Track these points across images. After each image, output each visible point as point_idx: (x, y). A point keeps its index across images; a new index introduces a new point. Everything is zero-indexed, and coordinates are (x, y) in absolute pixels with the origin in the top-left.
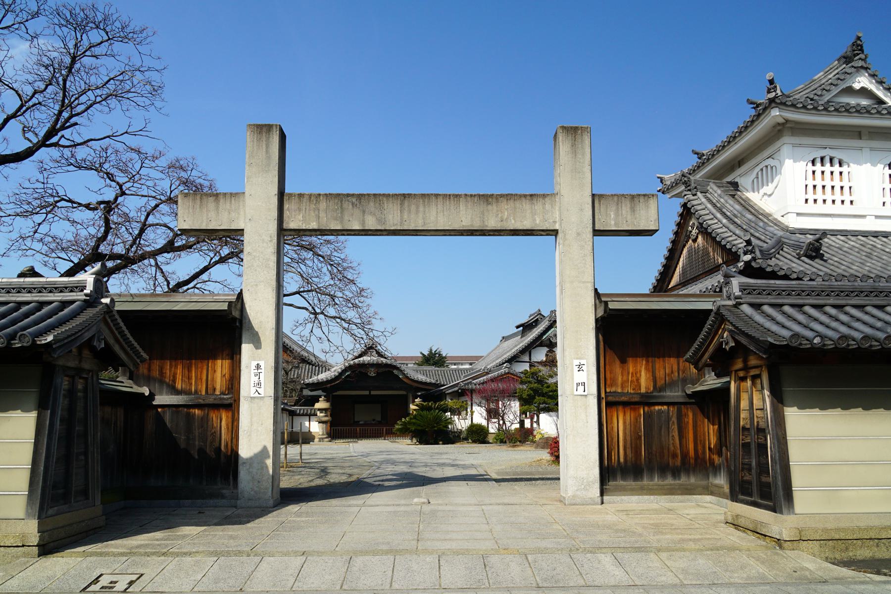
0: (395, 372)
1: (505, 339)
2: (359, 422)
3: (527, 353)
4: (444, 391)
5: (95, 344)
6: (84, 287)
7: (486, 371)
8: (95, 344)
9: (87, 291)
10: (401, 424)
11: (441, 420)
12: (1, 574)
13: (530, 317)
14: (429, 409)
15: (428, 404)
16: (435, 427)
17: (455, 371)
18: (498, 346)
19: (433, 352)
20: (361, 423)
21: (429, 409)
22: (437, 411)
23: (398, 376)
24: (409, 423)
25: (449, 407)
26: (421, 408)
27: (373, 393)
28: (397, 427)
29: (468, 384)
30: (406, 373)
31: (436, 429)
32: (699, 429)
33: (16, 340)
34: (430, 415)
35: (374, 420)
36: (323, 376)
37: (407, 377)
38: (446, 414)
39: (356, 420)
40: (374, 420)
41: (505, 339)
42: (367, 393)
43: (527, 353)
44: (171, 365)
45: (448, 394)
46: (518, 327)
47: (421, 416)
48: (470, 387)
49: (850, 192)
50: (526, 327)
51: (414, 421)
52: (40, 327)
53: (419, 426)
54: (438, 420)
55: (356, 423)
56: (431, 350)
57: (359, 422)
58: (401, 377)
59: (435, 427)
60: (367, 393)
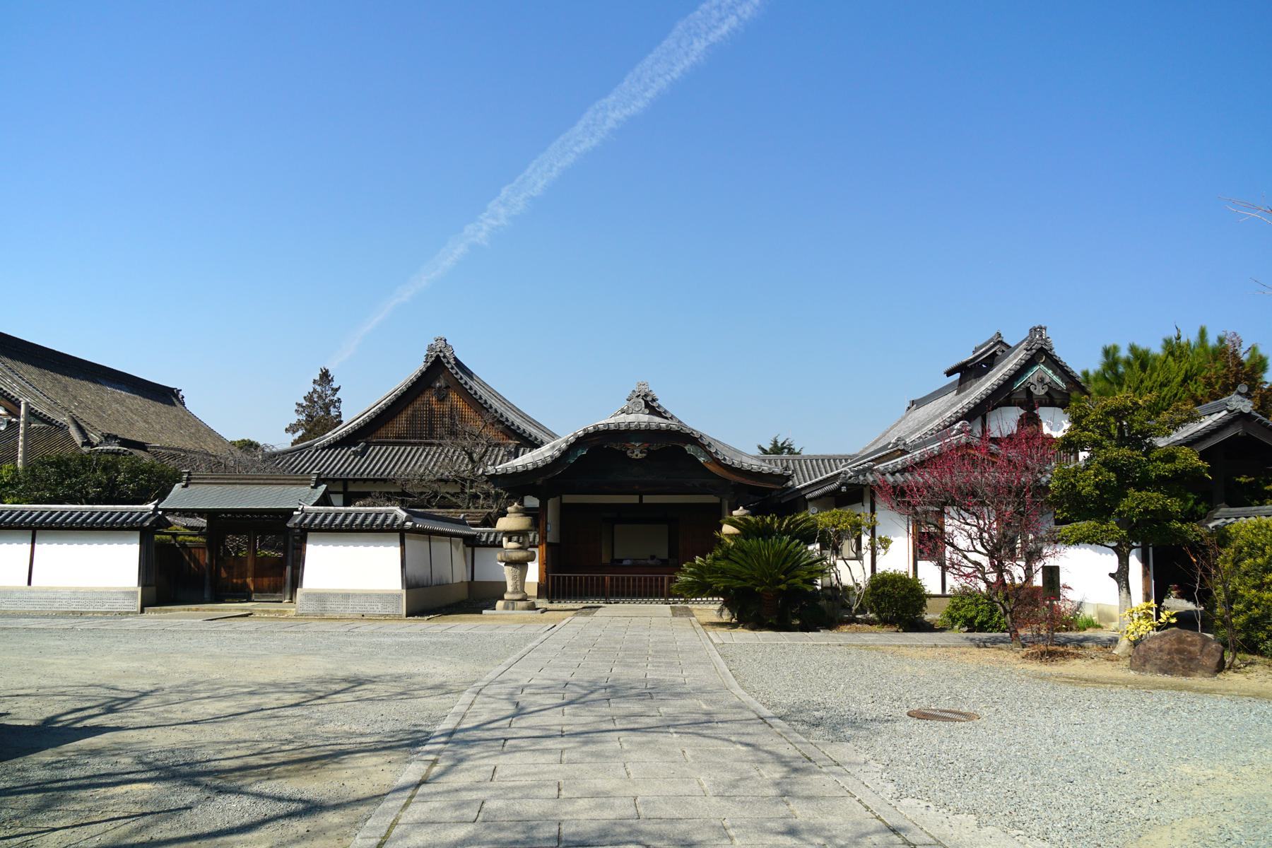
0: (689, 449)
1: (916, 404)
2: (621, 561)
3: (979, 419)
4: (803, 493)
7: (901, 447)
10: (692, 573)
11: (796, 565)
13: (974, 352)
14: (766, 533)
15: (763, 520)
16: (780, 582)
17: (823, 460)
18: (904, 418)
19: (779, 445)
20: (625, 563)
21: (766, 533)
22: (786, 538)
23: (694, 459)
24: (711, 570)
25: (820, 527)
26: (747, 530)
27: (648, 499)
28: (682, 578)
29: (864, 472)
30: (713, 451)
31: (783, 587)
34: (767, 548)
35: (653, 557)
36: (527, 459)
37: (717, 462)
38: (810, 548)
39: (616, 557)
40: (653, 557)
41: (916, 404)
42: (634, 499)
43: (979, 419)
44: (908, 575)
45: (811, 500)
46: (949, 373)
47: (743, 551)
48: (870, 478)
50: (968, 372)
51: (723, 563)
53: (738, 578)
54: (790, 564)
55: (616, 564)
56: (776, 442)
57: (621, 561)
58: (702, 460)
59: (780, 582)
60: (634, 499)
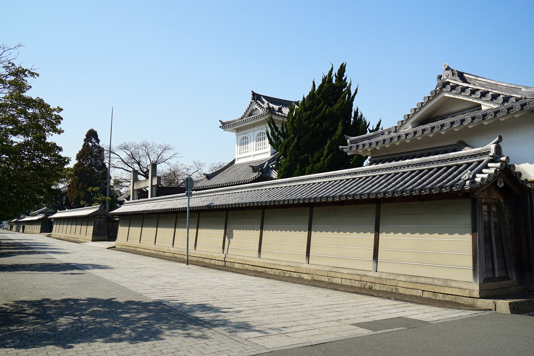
5: (498, 185)
6: (489, 152)
8: (498, 185)
9: (491, 154)
12: (1, 124)
32: (478, 227)
33: (454, 187)
49: (358, 86)
52: (389, 182)
